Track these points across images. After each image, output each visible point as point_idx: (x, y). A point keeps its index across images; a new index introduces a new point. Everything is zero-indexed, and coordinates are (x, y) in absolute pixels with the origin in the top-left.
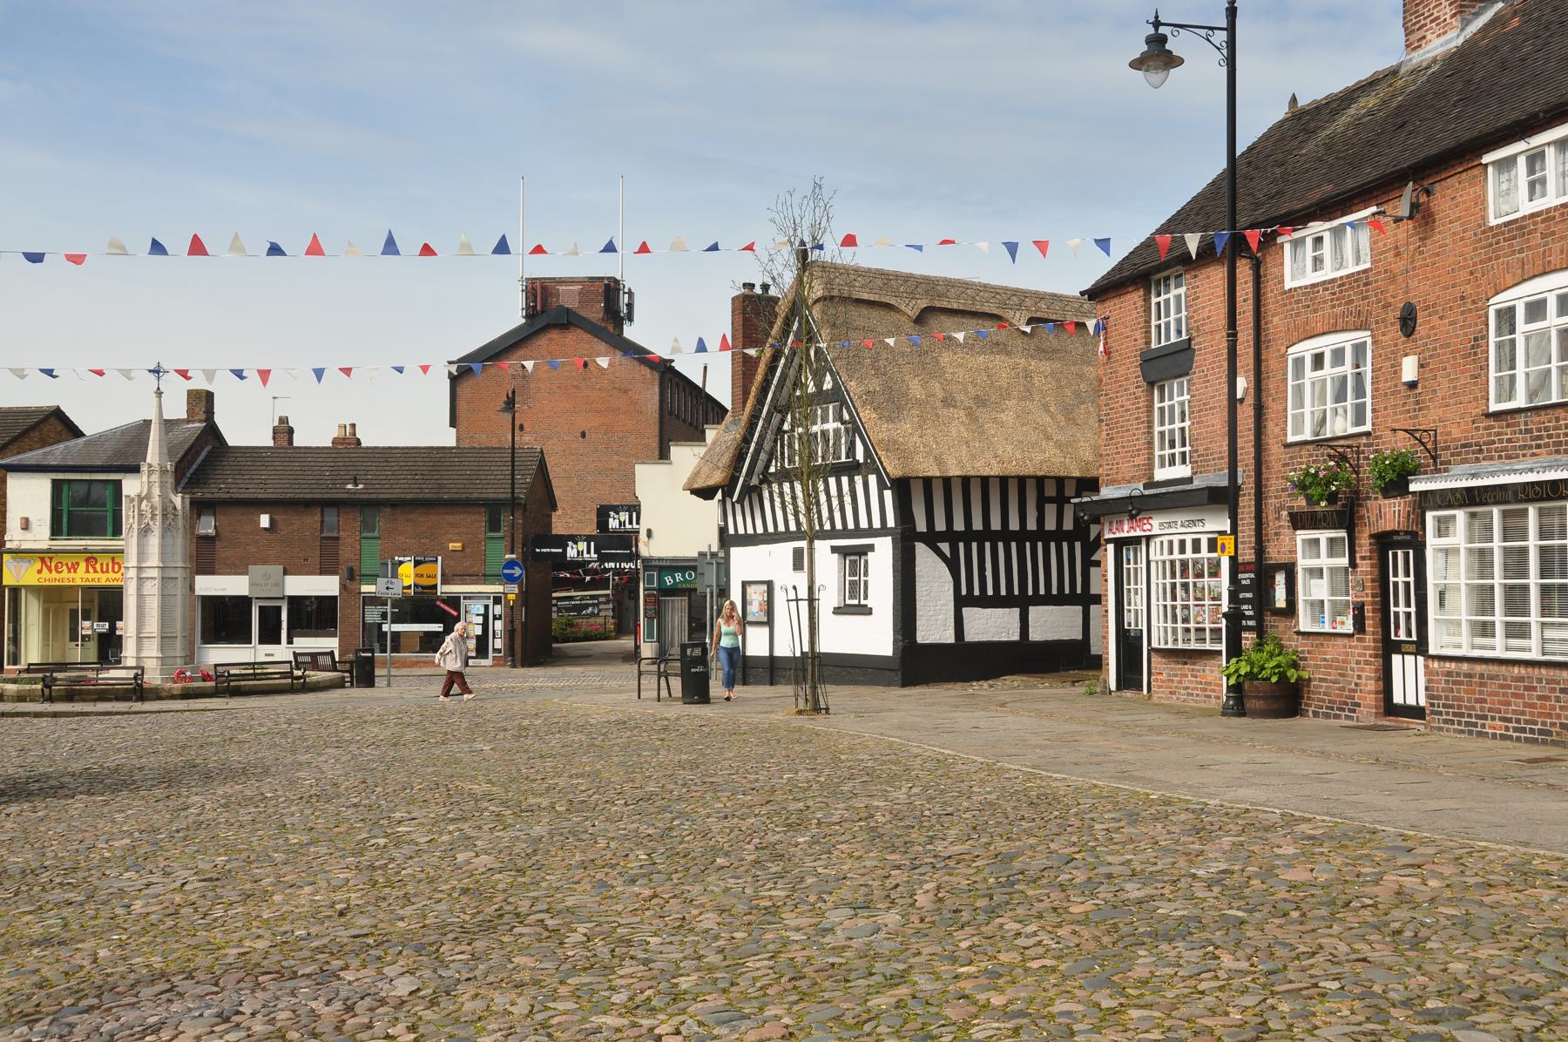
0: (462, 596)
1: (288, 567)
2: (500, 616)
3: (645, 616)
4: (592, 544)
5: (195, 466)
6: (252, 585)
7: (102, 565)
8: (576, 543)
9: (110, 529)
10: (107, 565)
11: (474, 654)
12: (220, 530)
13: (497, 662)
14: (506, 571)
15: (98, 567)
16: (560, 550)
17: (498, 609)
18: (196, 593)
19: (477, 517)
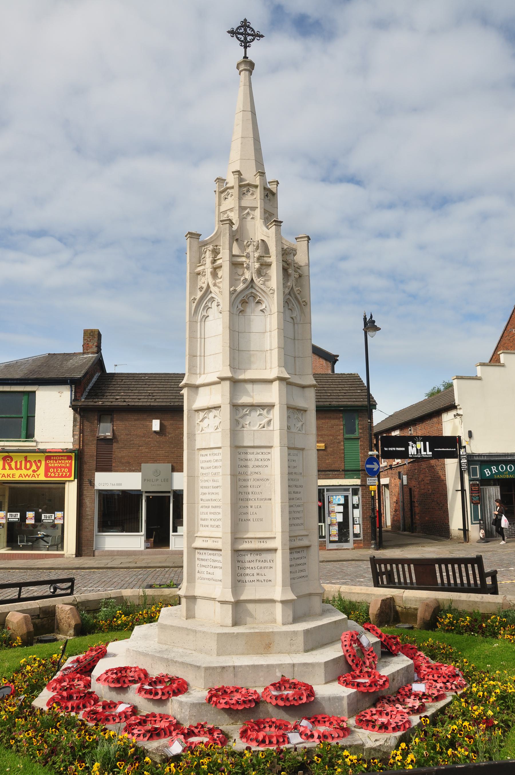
0: (325, 488)
1: (175, 465)
2: (358, 505)
3: (472, 502)
4: (427, 443)
5: (91, 385)
6: (144, 480)
7: (16, 462)
8: (415, 443)
9: (24, 433)
10: (21, 462)
11: (336, 539)
12: (116, 433)
13: (358, 545)
14: (368, 466)
15: (13, 464)
16: (403, 449)
17: (356, 500)
18: (95, 488)
19: (336, 422)
